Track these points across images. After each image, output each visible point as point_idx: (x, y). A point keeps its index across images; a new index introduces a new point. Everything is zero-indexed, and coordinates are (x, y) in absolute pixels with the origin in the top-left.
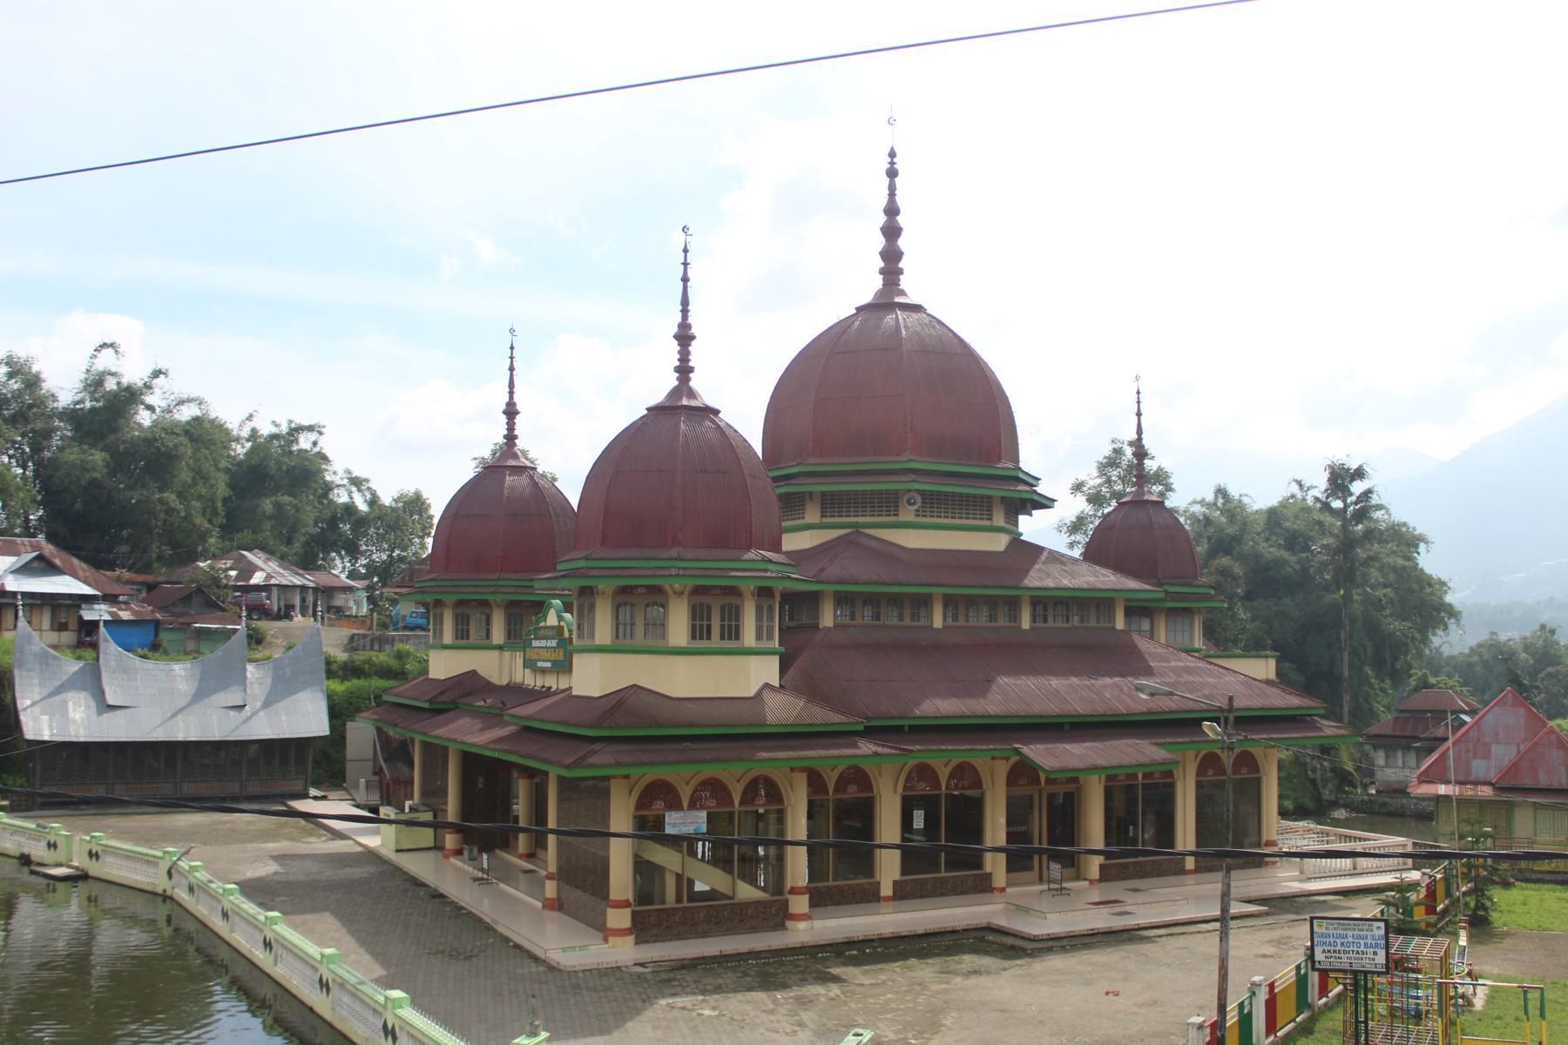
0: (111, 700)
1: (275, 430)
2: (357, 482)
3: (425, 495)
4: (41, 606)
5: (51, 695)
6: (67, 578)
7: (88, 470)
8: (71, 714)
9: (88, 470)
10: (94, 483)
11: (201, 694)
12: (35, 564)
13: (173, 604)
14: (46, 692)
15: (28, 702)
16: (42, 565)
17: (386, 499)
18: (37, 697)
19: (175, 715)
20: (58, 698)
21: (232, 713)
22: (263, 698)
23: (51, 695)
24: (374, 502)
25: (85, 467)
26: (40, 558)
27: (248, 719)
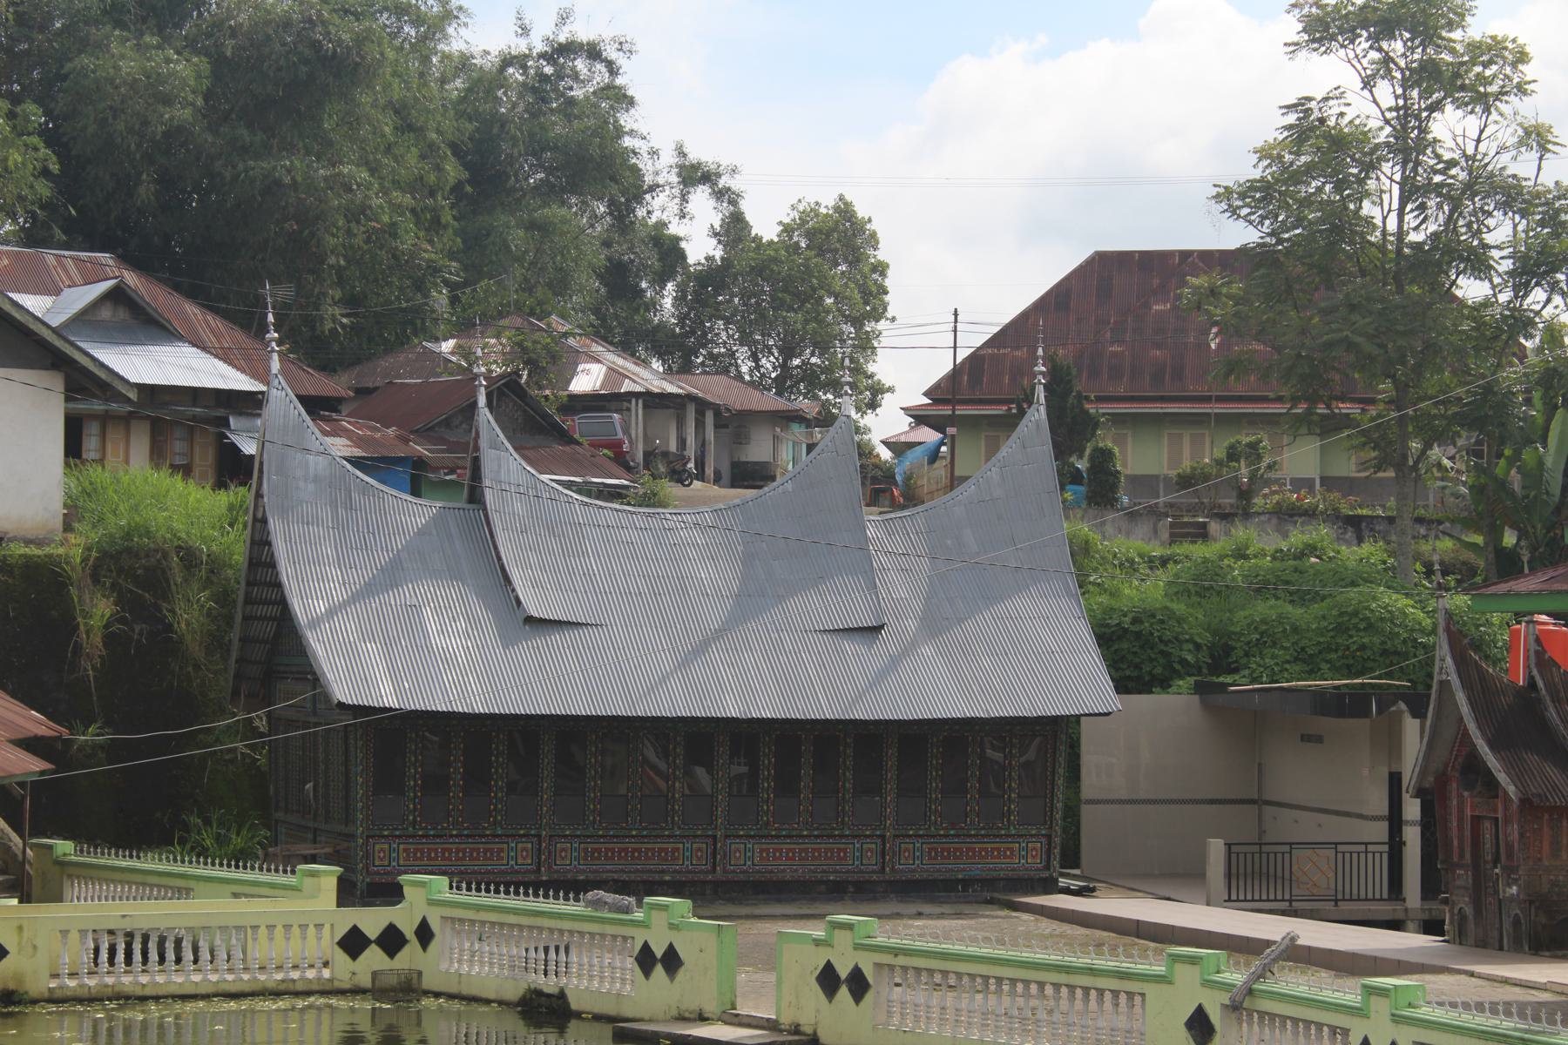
0: (534, 606)
1: (520, 46)
2: (694, 175)
3: (861, 212)
4: (126, 420)
5: (369, 590)
6: (188, 351)
7: (167, 101)
8: (437, 641)
9: (167, 101)
10: (176, 133)
11: (754, 598)
12: (106, 313)
13: (447, 423)
14: (360, 577)
15: (321, 607)
16: (123, 314)
17: (766, 224)
18: (339, 595)
19: (702, 648)
20: (394, 598)
21: (849, 646)
22: (918, 605)
23: (369, 590)
24: (734, 228)
25: (157, 92)
26: (118, 296)
27: (894, 663)
